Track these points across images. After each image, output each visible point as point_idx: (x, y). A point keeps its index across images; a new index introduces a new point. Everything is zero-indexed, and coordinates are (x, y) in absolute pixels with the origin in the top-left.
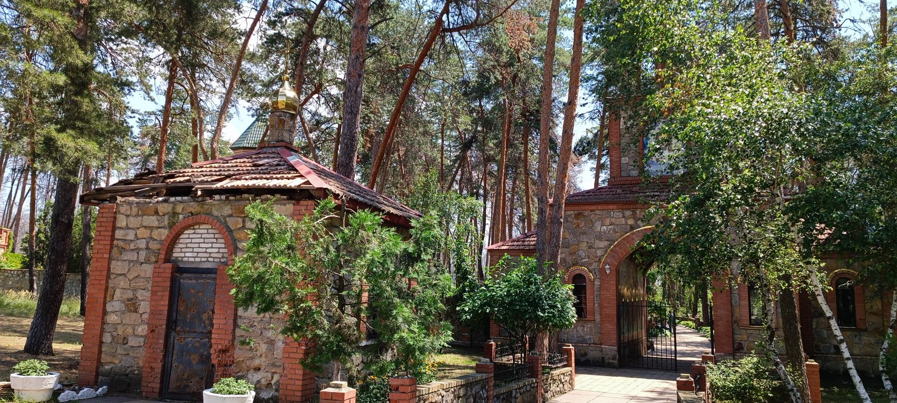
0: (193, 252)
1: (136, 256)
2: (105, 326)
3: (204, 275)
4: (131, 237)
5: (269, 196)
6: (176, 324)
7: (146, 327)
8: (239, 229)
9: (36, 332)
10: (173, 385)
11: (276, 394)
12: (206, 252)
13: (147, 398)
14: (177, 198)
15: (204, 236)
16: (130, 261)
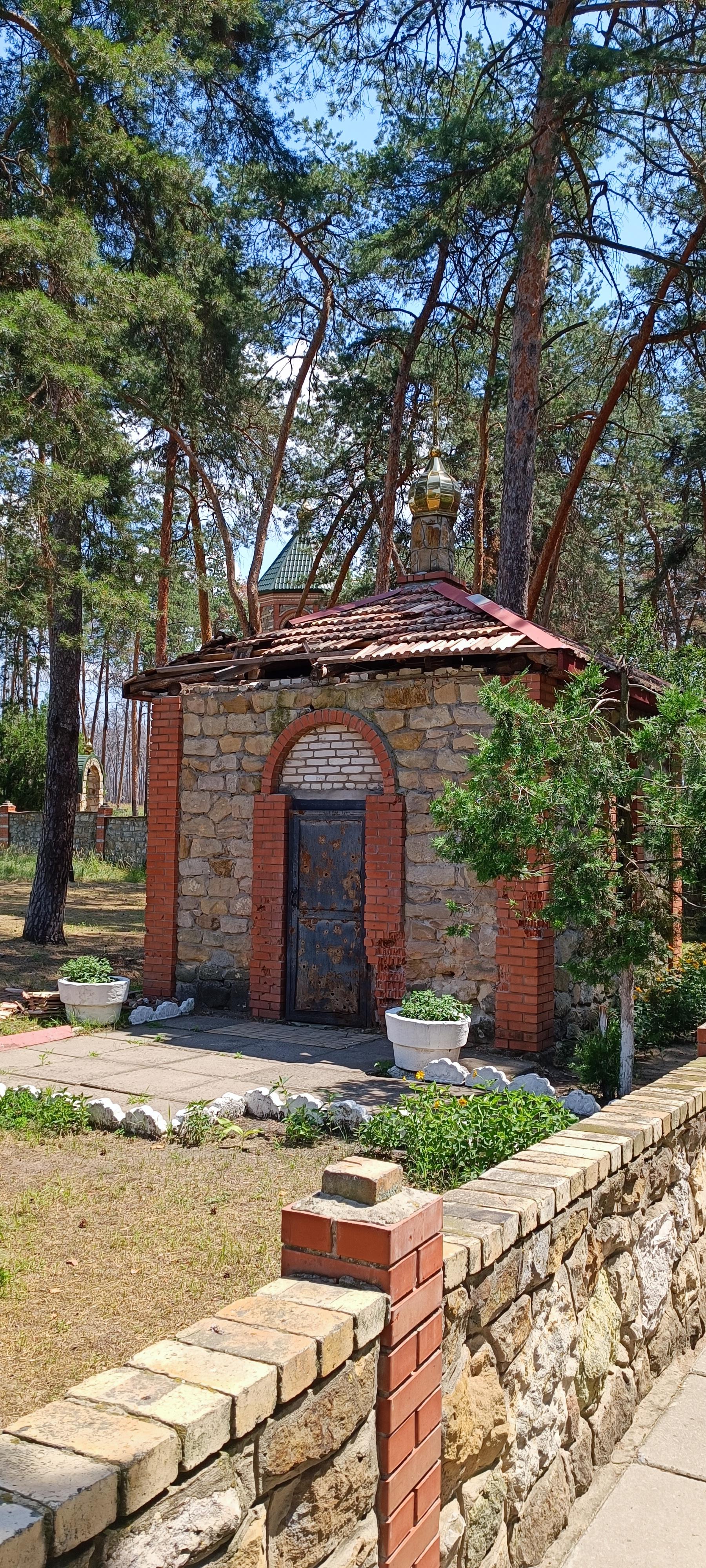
0: (317, 773)
1: (222, 783)
2: (180, 900)
3: (340, 813)
4: (210, 749)
5: (450, 669)
6: (299, 895)
7: (249, 901)
8: (399, 731)
9: (39, 909)
10: (302, 1000)
11: (488, 1018)
12: (340, 773)
13: (261, 1019)
14: (282, 681)
15: (334, 745)
16: (213, 792)
